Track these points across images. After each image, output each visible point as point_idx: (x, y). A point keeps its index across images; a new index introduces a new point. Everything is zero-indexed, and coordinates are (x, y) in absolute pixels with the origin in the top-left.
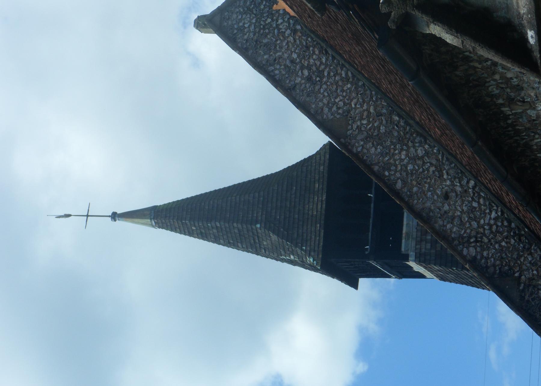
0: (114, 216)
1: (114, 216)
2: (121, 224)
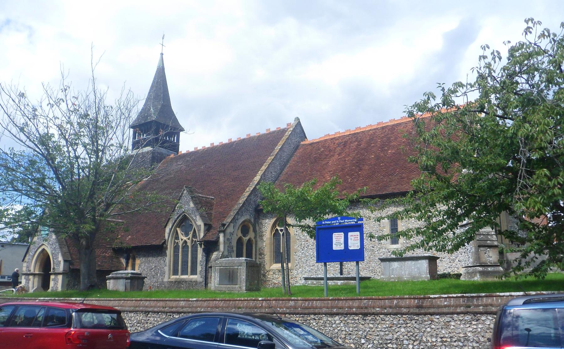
0: (162, 54)
1: (162, 54)
2: (159, 56)
